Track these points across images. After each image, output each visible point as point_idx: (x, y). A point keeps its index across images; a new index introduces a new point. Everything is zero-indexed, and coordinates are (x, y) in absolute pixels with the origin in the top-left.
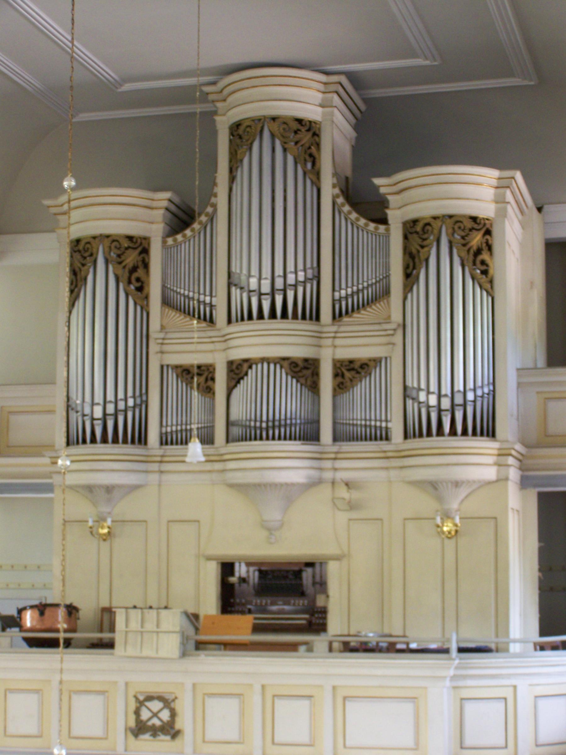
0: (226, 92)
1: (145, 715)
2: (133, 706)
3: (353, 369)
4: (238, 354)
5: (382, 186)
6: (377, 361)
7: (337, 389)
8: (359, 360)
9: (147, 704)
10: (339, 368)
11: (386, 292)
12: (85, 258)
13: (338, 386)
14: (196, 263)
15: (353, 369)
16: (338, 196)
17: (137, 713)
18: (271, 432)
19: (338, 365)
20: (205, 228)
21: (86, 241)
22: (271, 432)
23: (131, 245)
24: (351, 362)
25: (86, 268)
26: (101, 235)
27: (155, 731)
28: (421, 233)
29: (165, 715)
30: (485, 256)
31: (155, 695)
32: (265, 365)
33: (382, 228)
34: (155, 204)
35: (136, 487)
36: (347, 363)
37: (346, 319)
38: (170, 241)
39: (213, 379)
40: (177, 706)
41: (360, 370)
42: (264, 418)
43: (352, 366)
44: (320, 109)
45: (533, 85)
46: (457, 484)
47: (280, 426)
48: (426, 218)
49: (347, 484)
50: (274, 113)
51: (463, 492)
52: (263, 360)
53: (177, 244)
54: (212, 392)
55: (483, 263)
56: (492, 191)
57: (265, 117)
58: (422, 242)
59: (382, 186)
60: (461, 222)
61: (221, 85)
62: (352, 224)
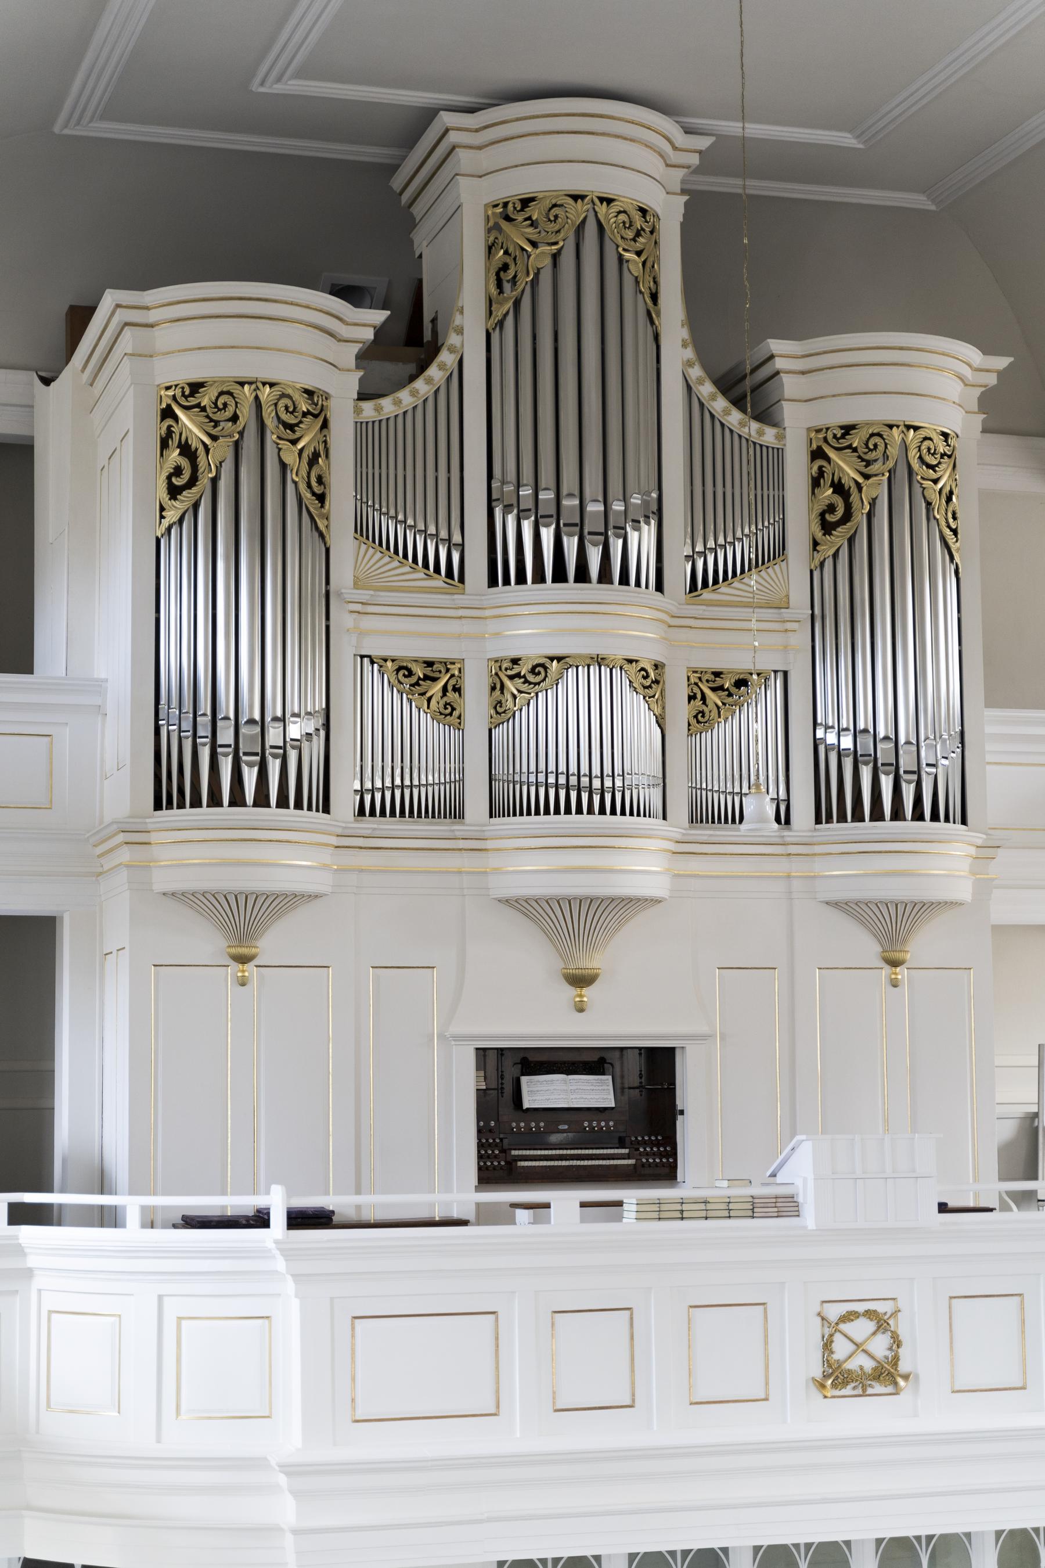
1: (841, 1348)
2: (815, 1331)
3: (721, 688)
5: (781, 356)
7: (694, 722)
9: (842, 1327)
10: (696, 684)
12: (216, 424)
13: (696, 717)
16: (689, 364)
17: (827, 1346)
22: (250, 778)
23: (862, 450)
28: (862, 450)
29: (880, 1346)
34: (344, 331)
37: (707, 595)
42: (552, 767)
43: (719, 682)
54: (456, 713)
58: (866, 466)
59: (781, 356)
60: (930, 439)
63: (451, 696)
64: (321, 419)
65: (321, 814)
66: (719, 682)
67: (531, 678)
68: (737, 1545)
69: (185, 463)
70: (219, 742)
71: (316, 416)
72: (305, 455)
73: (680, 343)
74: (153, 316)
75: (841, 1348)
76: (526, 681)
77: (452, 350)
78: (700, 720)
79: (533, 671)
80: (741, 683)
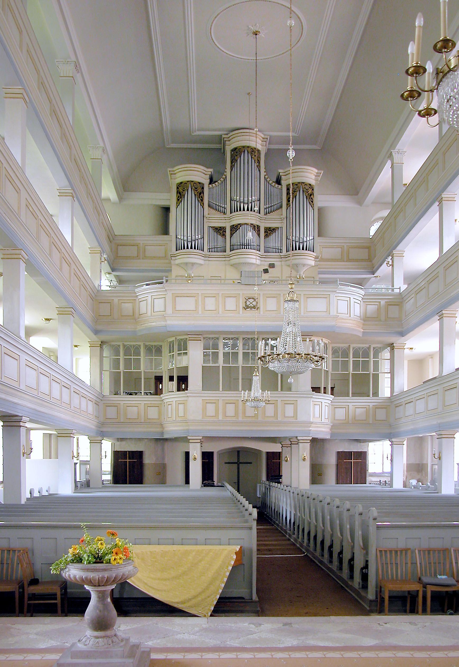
0: (231, 138)
1: (248, 303)
3: (270, 230)
4: (235, 222)
6: (278, 228)
8: (272, 227)
9: (248, 300)
11: (281, 207)
13: (266, 235)
14: (221, 193)
15: (270, 230)
17: (246, 302)
18: (246, 247)
19: (266, 229)
20: (222, 183)
21: (185, 183)
22: (246, 247)
24: (270, 228)
25: (185, 191)
26: (190, 181)
27: (251, 308)
30: (312, 196)
31: (251, 298)
32: (246, 225)
33: (280, 186)
34: (206, 173)
35: (201, 265)
36: (268, 228)
38: (210, 185)
39: (225, 232)
40: (258, 300)
41: (273, 231)
43: (270, 229)
44: (261, 146)
45: (319, 149)
46: (304, 265)
47: (248, 245)
48: (296, 183)
49: (457, 131)
50: (248, 145)
51: (305, 268)
52: (245, 224)
53: (213, 188)
55: (312, 199)
56: (314, 177)
57: (246, 146)
61: (229, 135)
62: (270, 184)
63: (224, 233)
64: (312, 189)
65: (202, 251)
66: (270, 229)
67: (235, 228)
68: (157, 236)
69: (180, 195)
70: (188, 241)
71: (311, 188)
72: (199, 193)
73: (264, 172)
74: (175, 172)
75: (248, 303)
76: (235, 228)
77: (225, 175)
78: (266, 236)
79: (236, 227)
80: (273, 229)
